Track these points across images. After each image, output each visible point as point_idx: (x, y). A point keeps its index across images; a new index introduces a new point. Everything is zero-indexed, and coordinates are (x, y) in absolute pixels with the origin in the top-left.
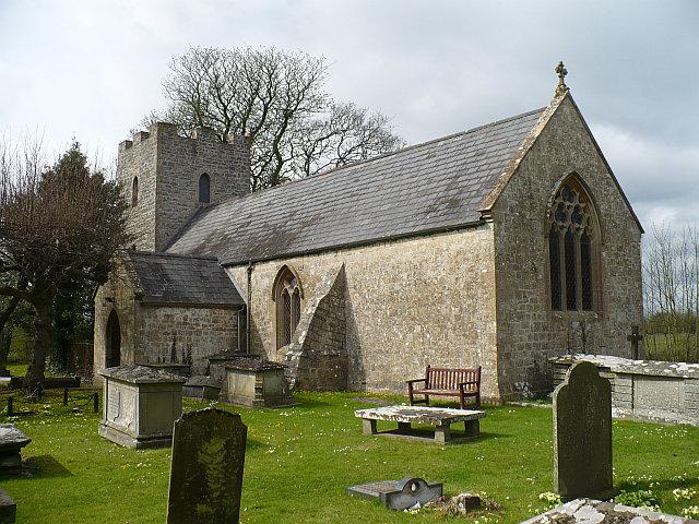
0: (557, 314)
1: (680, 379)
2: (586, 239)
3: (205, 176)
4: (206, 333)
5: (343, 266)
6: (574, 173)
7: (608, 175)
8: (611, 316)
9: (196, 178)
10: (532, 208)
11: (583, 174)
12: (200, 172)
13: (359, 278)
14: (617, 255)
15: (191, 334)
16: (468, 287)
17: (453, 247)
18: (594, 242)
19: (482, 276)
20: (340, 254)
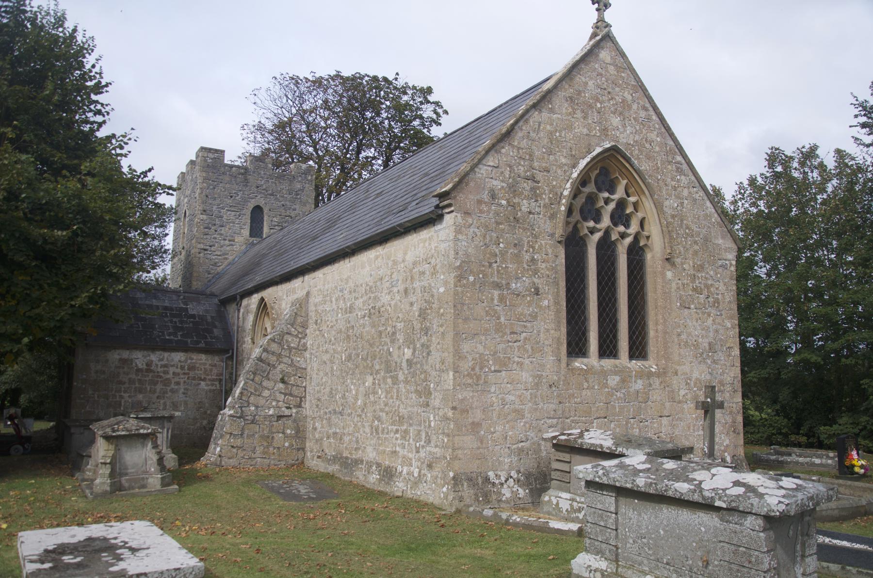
0: (578, 363)
1: (708, 506)
2: (636, 253)
3: (257, 211)
4: (178, 383)
5: (308, 294)
6: (614, 149)
7: (679, 158)
8: (681, 369)
9: (248, 212)
10: (535, 195)
11: (634, 154)
12: (251, 205)
13: (320, 308)
14: (694, 278)
15: (156, 383)
16: (423, 314)
17: (410, 258)
18: (653, 258)
19: (438, 299)
20: (307, 277)
